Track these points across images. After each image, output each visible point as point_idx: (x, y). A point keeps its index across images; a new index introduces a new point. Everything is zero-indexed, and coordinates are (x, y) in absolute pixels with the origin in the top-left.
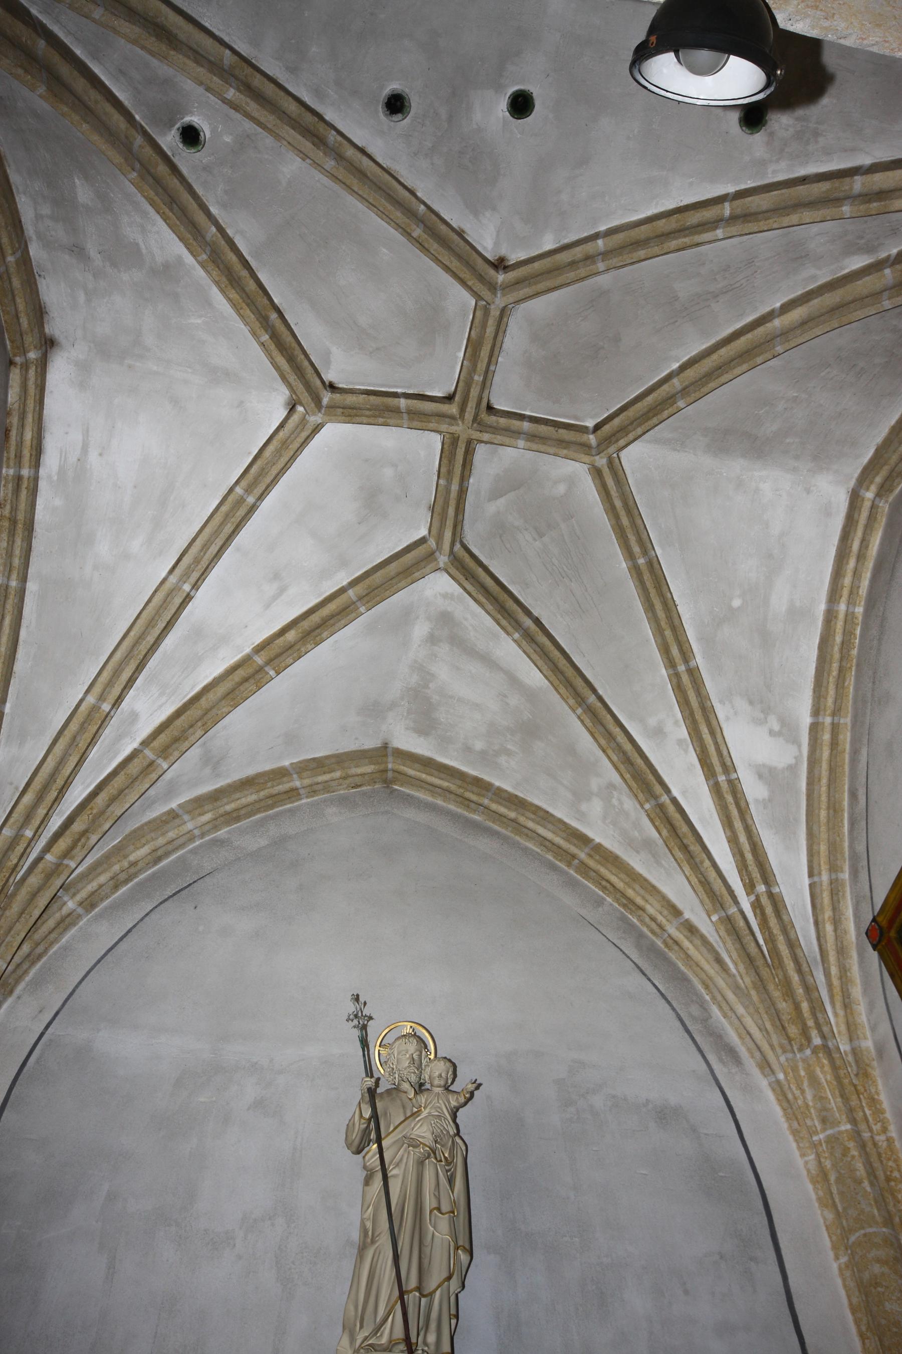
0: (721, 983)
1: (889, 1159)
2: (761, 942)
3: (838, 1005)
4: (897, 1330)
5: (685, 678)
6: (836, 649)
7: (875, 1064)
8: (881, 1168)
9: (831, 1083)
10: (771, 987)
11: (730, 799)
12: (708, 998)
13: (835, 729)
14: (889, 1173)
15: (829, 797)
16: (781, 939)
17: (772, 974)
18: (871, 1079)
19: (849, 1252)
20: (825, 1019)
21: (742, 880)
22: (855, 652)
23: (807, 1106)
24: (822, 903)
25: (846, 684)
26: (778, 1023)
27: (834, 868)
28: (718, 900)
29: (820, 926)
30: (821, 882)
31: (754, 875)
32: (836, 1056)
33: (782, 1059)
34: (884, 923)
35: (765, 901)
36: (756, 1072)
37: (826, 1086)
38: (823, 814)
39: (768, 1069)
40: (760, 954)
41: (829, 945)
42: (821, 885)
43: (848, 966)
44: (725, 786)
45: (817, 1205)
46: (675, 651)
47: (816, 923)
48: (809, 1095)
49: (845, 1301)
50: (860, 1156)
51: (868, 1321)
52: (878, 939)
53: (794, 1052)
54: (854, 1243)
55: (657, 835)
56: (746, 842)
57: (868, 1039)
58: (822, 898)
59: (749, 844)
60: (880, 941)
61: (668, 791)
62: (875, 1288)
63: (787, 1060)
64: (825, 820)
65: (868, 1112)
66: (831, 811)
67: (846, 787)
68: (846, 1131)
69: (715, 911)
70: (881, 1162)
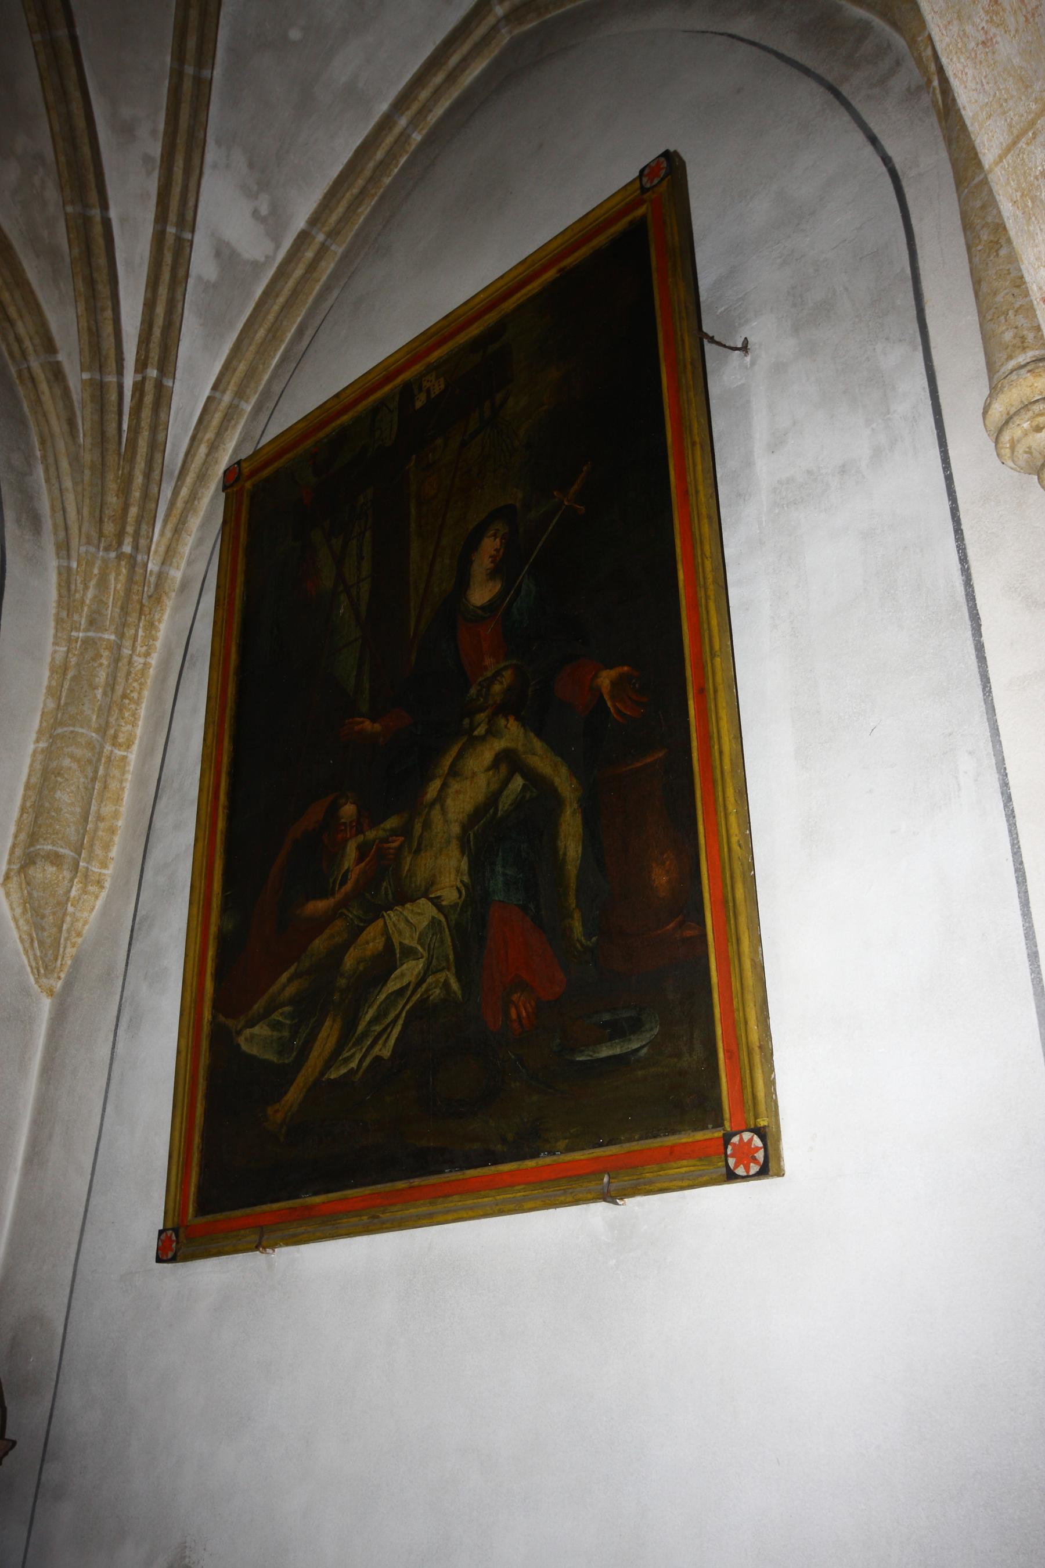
0: (61, 446)
1: (136, 681)
2: (125, 427)
3: (170, 526)
4: (56, 815)
5: (187, 85)
6: (371, 165)
7: (173, 595)
8: (123, 684)
9: (119, 592)
10: (110, 476)
11: (168, 258)
12: (38, 454)
13: (323, 250)
14: (128, 692)
15: (277, 318)
16: (145, 434)
17: (119, 464)
18: (161, 606)
19: (51, 741)
20: (148, 532)
21: (138, 352)
22: (387, 181)
23: (83, 602)
24: (210, 422)
25: (360, 210)
26: (97, 514)
27: (240, 394)
28: (100, 360)
29: (196, 443)
30: (220, 401)
31: (152, 354)
32: (139, 571)
33: (83, 549)
34: (246, 469)
35: (149, 387)
36: (50, 549)
37: (112, 593)
38: (261, 333)
39: (65, 552)
40: (117, 438)
41: (193, 466)
42: (219, 404)
43: (200, 494)
44: (170, 240)
45: (44, 691)
46: (191, 43)
47: (193, 438)
48: (90, 594)
49: (24, 778)
50: (109, 666)
51: (36, 800)
52: (232, 482)
53: (99, 549)
54: (58, 734)
55: (68, 251)
56: (162, 315)
57: (180, 570)
58: (212, 417)
59: (165, 319)
60: (232, 485)
61: (105, 206)
62: (56, 777)
63: (87, 552)
64: (260, 341)
65: (141, 633)
66: (270, 335)
67: (299, 319)
68: (109, 640)
69: (89, 369)
70: (127, 680)
